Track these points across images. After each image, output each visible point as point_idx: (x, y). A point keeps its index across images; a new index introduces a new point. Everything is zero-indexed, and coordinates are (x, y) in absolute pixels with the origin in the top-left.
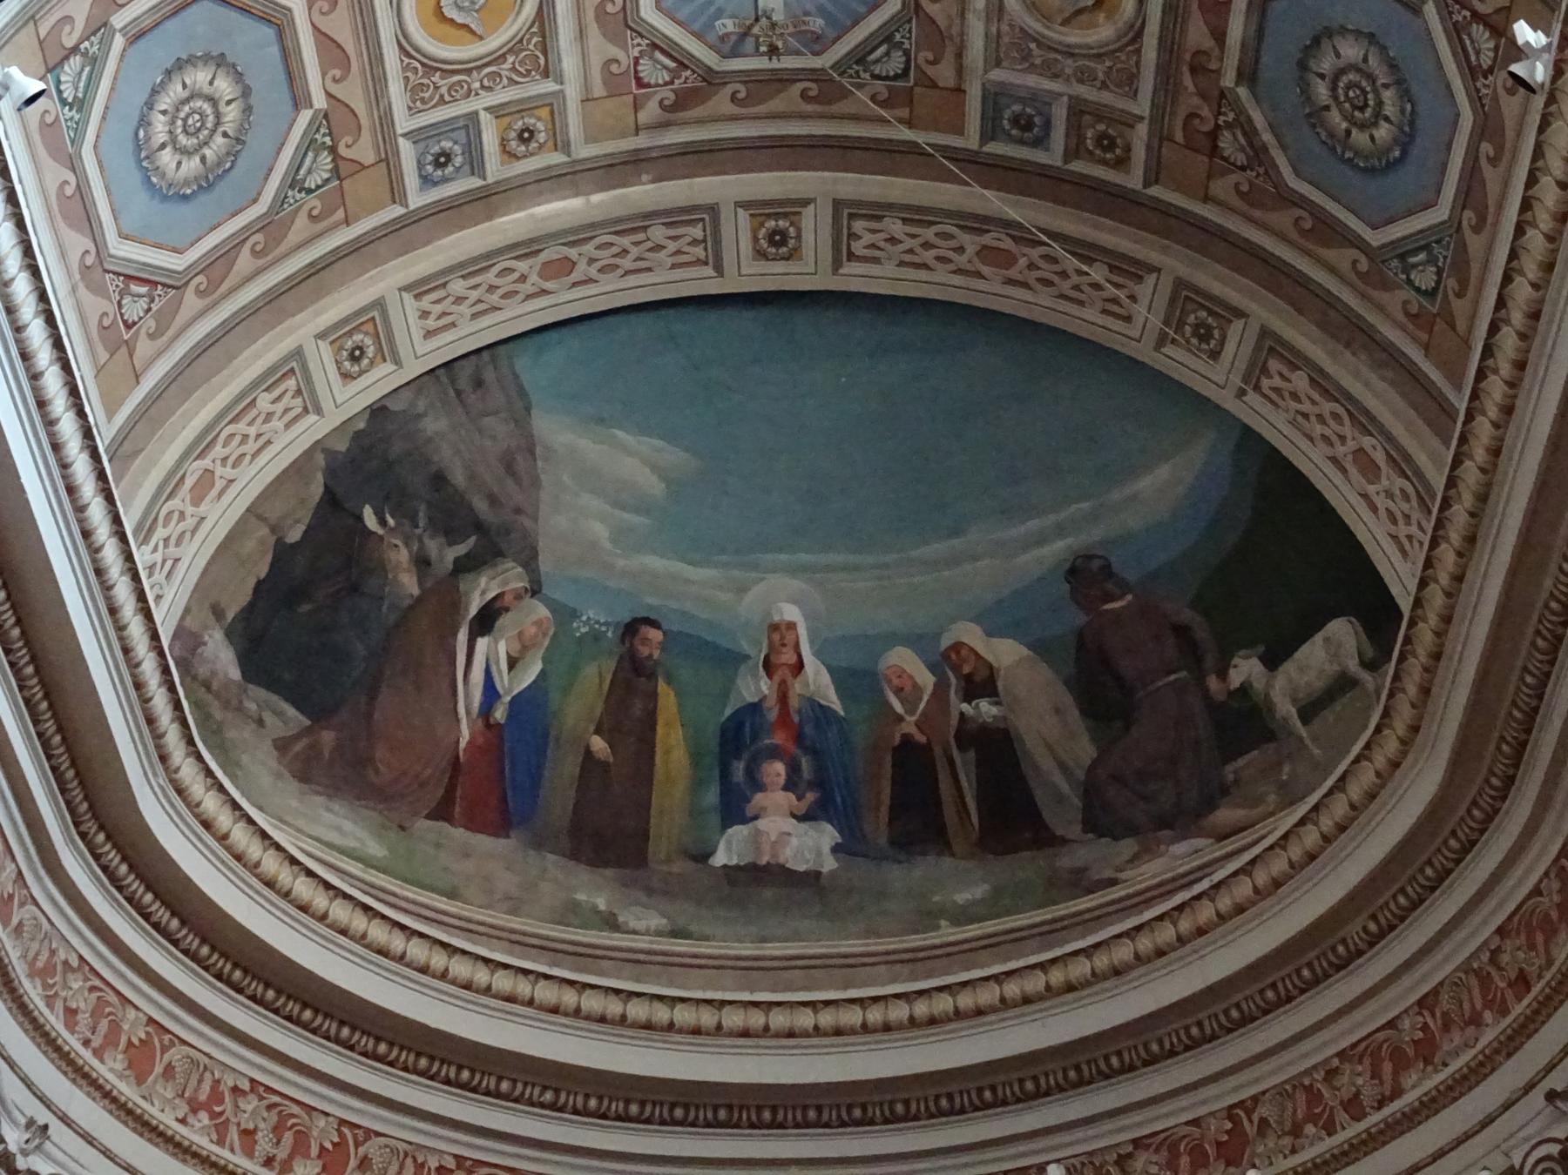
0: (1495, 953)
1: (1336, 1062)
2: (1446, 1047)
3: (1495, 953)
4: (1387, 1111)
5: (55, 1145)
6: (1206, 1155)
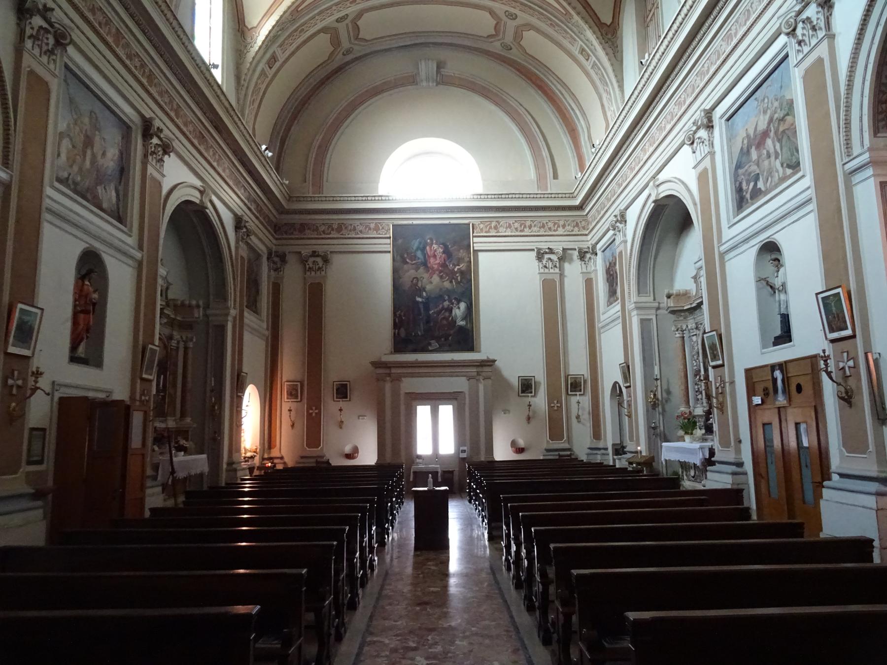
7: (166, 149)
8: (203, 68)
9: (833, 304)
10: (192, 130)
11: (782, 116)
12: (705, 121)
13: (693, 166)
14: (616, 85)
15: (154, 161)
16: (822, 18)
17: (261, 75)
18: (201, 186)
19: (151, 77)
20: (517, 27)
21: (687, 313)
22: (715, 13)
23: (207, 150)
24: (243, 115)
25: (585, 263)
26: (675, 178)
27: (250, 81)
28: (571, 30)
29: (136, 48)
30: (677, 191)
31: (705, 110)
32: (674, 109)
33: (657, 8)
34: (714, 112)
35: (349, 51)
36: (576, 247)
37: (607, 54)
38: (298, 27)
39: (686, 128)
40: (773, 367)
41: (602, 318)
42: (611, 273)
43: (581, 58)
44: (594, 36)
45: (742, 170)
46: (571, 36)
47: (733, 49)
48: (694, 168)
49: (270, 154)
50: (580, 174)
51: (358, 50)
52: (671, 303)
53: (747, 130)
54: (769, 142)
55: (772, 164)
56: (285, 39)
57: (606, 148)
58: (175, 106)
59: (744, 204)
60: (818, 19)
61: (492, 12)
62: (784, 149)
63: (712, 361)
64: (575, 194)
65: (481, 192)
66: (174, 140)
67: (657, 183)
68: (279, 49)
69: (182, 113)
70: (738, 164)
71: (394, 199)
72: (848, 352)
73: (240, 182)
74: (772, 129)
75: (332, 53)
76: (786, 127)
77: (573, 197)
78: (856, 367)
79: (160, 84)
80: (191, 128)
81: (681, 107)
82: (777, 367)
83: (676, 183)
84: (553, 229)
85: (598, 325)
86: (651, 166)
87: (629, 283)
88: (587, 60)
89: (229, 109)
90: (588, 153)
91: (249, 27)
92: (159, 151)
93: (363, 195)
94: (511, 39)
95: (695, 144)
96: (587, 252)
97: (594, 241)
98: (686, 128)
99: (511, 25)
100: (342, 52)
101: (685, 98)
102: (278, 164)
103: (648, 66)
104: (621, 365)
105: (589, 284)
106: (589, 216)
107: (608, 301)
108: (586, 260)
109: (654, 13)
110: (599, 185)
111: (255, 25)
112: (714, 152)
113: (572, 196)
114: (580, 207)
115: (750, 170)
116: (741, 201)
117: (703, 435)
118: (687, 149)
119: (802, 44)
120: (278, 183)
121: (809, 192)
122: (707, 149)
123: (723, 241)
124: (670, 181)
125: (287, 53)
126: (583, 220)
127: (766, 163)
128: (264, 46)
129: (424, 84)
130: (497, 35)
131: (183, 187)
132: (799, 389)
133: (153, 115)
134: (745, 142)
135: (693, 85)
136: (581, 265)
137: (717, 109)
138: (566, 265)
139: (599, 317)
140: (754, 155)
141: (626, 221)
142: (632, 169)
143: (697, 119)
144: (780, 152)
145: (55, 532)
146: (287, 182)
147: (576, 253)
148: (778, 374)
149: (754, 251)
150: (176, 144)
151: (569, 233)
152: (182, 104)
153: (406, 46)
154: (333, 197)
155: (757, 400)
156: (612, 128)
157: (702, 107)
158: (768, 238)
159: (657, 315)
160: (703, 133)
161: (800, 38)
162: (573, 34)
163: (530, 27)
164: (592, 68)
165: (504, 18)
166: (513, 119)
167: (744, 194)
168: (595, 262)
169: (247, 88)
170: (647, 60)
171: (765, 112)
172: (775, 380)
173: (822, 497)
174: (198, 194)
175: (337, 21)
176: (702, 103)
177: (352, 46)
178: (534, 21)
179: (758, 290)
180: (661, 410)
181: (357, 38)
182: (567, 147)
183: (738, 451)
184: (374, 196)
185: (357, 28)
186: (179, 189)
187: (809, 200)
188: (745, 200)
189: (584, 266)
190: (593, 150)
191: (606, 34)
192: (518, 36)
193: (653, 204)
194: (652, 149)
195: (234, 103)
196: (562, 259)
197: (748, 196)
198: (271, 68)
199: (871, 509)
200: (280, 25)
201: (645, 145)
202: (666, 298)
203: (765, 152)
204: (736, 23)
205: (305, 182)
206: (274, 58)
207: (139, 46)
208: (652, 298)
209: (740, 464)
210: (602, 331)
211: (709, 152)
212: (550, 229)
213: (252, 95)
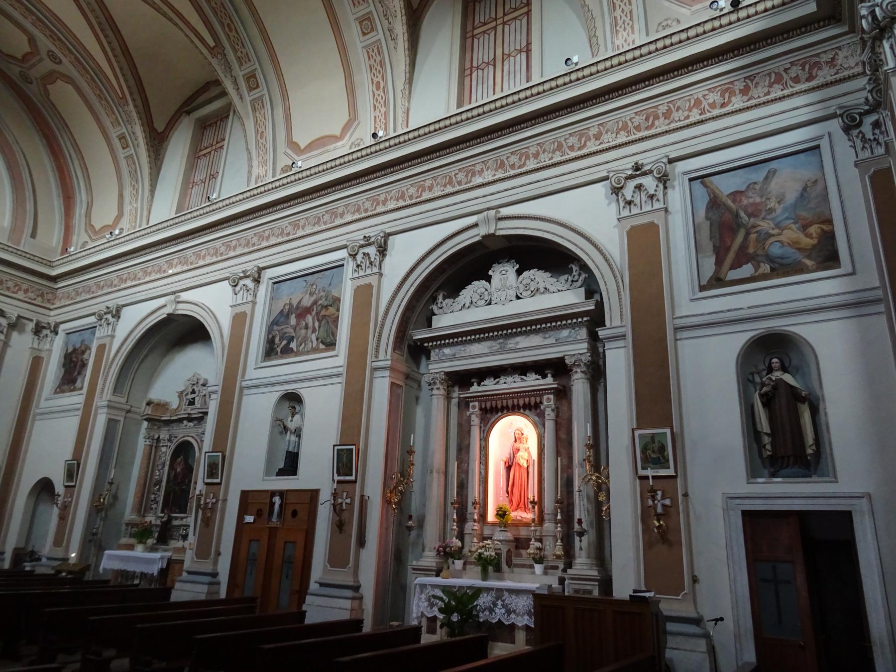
0: (323, 215)
1: (568, 136)
2: (436, 189)
3: (323, 215)
4: (466, 186)
5: (289, 446)
6: (590, 137)
9: (345, 455)
11: (325, 304)
12: (256, 276)
16: (378, 260)
21: (162, 424)
22: (292, 203)
25: (38, 339)
30: (202, 316)
36: (35, 319)
40: (273, 493)
41: (43, 404)
42: (74, 359)
43: (117, 143)
44: (144, 134)
45: (278, 327)
46: (117, 118)
52: (149, 411)
53: (291, 299)
54: (309, 318)
55: (308, 335)
59: (273, 354)
60: (375, 259)
61: (32, 40)
62: (322, 329)
63: (207, 478)
64: (54, 264)
70: (276, 321)
72: (347, 492)
74: (315, 309)
76: (327, 313)
77: (50, 266)
78: (351, 504)
82: (277, 494)
84: (12, 289)
85: (34, 410)
86: (177, 282)
87: (107, 376)
95: (238, 288)
96: (44, 328)
97: (59, 319)
104: (67, 462)
105: (36, 364)
106: (60, 291)
107: (59, 387)
108: (41, 335)
112: (256, 303)
113: (50, 264)
114: (54, 279)
115: (285, 330)
116: (270, 351)
117: (153, 544)
119: (360, 268)
121: (341, 369)
122: (250, 298)
123: (246, 378)
126: (51, 292)
127: (303, 331)
132: (294, 514)
134: (287, 307)
136: (33, 339)
138: (15, 335)
139: (39, 401)
140: (293, 320)
141: (119, 317)
144: (317, 329)
145: (621, 602)
147: (31, 326)
148: (277, 500)
149: (277, 396)
151: (30, 301)
155: (249, 519)
158: (294, 389)
159: (125, 418)
160: (249, 282)
161: (359, 263)
162: (119, 118)
167: (276, 346)
168: (52, 341)
171: (311, 294)
172: (272, 504)
173: (304, 602)
179: (273, 427)
180: (103, 515)
183: (215, 563)
187: (340, 375)
188: (275, 352)
189: (36, 342)
191: (154, 140)
192: (50, 77)
193: (166, 316)
196: (13, 326)
197: (279, 350)
199: (346, 609)
202: (144, 404)
203: (304, 323)
208: (126, 401)
209: (215, 575)
210: (37, 418)
212: (8, 289)
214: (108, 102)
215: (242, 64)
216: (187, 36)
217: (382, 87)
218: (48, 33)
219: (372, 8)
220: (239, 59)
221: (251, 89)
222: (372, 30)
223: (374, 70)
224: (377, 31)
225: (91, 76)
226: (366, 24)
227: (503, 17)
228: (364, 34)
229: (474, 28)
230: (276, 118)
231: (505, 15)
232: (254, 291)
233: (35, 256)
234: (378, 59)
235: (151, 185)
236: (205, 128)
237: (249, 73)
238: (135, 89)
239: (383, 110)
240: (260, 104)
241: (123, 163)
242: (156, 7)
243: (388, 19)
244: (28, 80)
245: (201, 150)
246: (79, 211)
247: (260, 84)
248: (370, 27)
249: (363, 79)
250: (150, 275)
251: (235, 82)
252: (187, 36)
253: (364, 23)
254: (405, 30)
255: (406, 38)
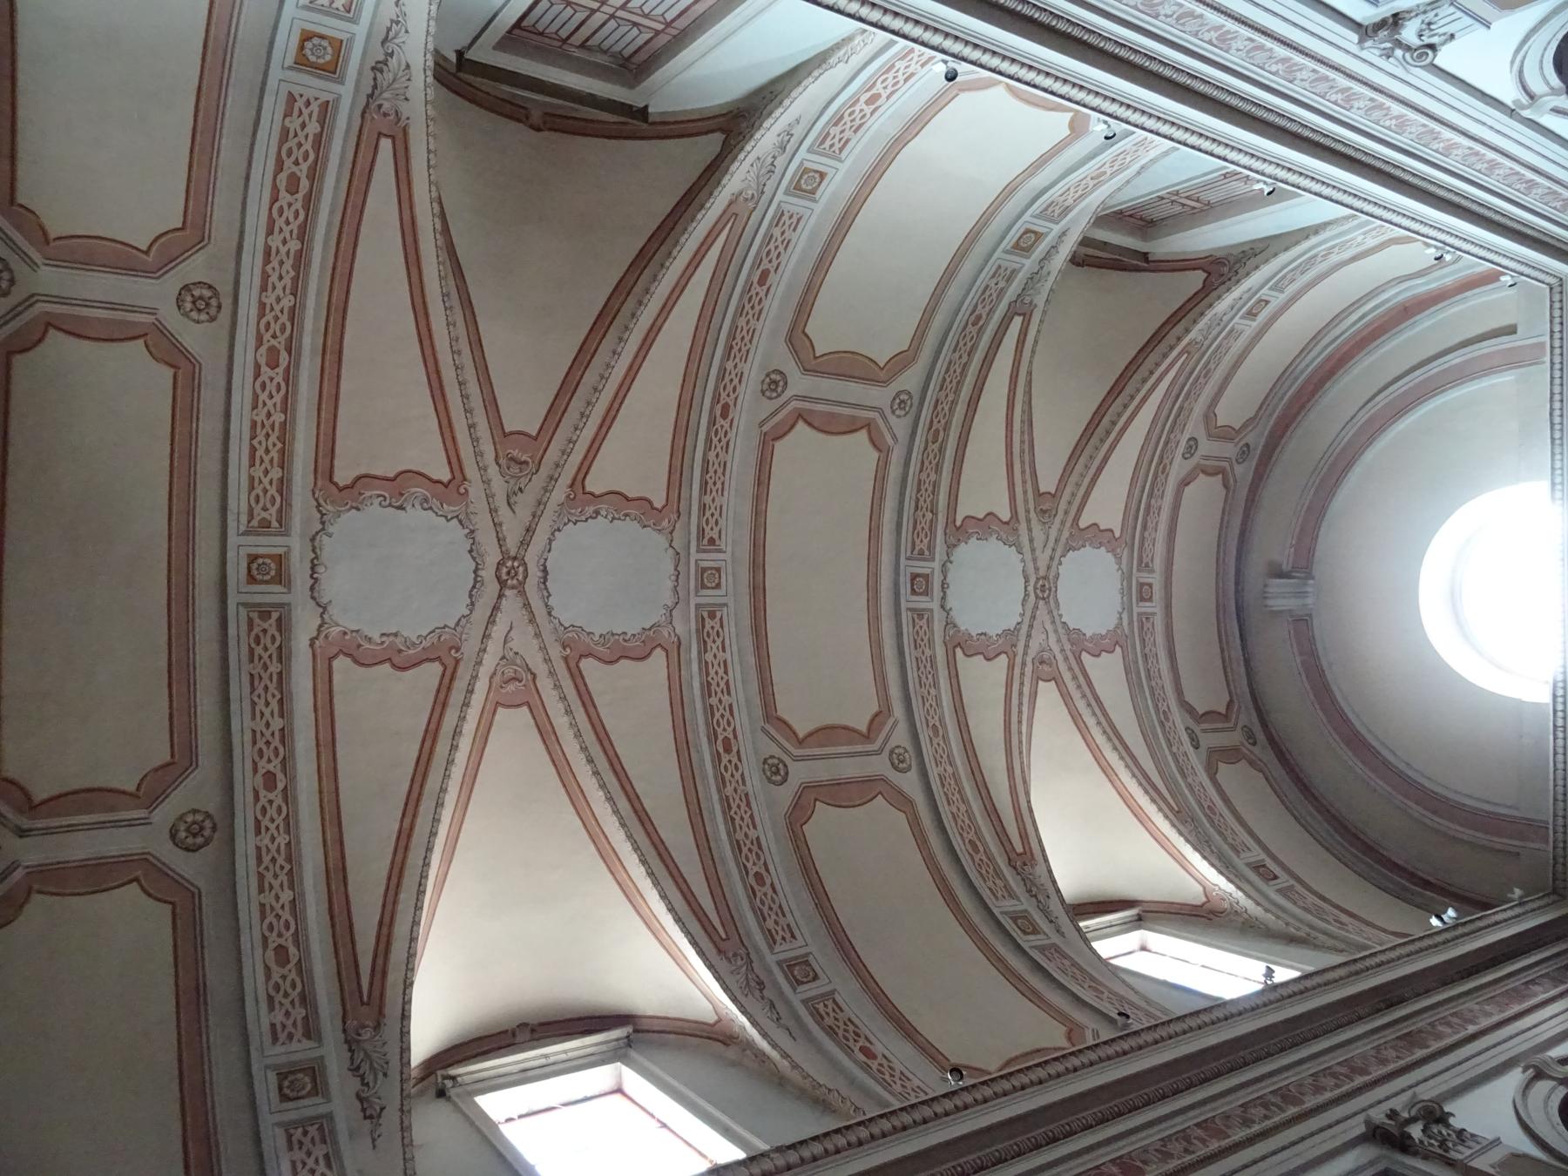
7: (1434, 1116)
8: (1273, 996)
10: (1264, 1111)
12: (1383, 34)
13: (1483, 29)
14: (1314, 240)
15: (1460, 1148)
17: (1285, 896)
18: (1524, 1072)
19: (1286, 1097)
20: (1210, 436)
23: (1439, 1037)
24: (1366, 947)
26: (1512, 62)
27: (1301, 921)
28: (1215, 339)
29: (1153, 1137)
30: (1545, 49)
31: (1361, 41)
32: (1238, 50)
33: (1177, 193)
34: (1366, 23)
35: (1251, 737)
37: (1257, 267)
38: (1206, 815)
39: (1399, 72)
46: (1225, 338)
47: (1411, 107)
48: (1487, 25)
49: (1451, 913)
50: (1503, 278)
51: (1248, 717)
56: (1225, 839)
57: (1444, 231)
58: (1343, 1070)
61: (1185, 482)
65: (1546, 484)
66: (1415, 1095)
67: (1525, 100)
68: (777, 948)
69: (1359, 1063)
71: (1561, 670)
73: (1514, 989)
75: (1252, 763)
79: (1301, 1085)
80: (1258, 1112)
81: (1296, 64)
83: (1524, 57)
88: (1267, 302)
89: (1354, 969)
90: (1473, 266)
91: (1204, 899)
92: (1440, 1133)
93: (1551, 737)
94: (1230, 445)
95: (1435, 40)
98: (1399, 72)
99: (1206, 447)
100: (1249, 747)
101: (1276, 63)
102: (1475, 902)
103: (1276, 179)
109: (1187, 198)
110: (1529, 232)
111: (1201, 889)
118: (1442, 59)
120: (1518, 910)
124: (1521, 72)
125: (1250, 842)
128: (1237, 880)
129: (1309, 601)
130: (868, 426)
131: (1526, 1106)
133: (1361, 1118)
135: (1248, 52)
137: (1358, 18)
142: (1493, 165)
143: (1377, 52)
146: (1518, 892)
150: (1427, 1092)
152: (1341, 1055)
153: (1241, 635)
154: (1555, 800)
156: (1409, 230)
157: (1354, 49)
160: (1409, 33)
163: (1209, 415)
164: (1282, 291)
165: (1195, 460)
166: (1382, 429)
169: (1312, 927)
170: (1265, 183)
174: (1543, 1086)
175: (1196, 747)
176: (1348, 52)
177: (1240, 725)
178: (1199, 408)
181: (1226, 717)
182: (1441, 317)
184: (1555, 711)
185: (1209, 715)
186: (1530, 1117)
190: (1448, 257)
194: (1447, 134)
195: (1340, 959)
198: (1276, 877)
200: (1203, 845)
201: (1436, 151)
204: (1200, 36)
205: (1518, 854)
206: (1258, 868)
207: (1228, 1099)
211: (1452, 4)
213: (1328, 922)
214: (1208, 362)
215: (1013, 271)
216: (1033, 352)
217: (868, 95)
218: (1161, 477)
219: (780, 196)
220: (1009, 280)
221: (1039, 236)
222: (806, 171)
223: (858, 122)
224: (801, 163)
225: (1183, 401)
226: (807, 184)
227: (598, 10)
228: (822, 175)
229: (657, 33)
230: (1055, 177)
231: (593, 11)
232: (1425, 12)
233: (1552, 317)
234: (835, 131)
235: (1307, 237)
236: (1152, 221)
237: (1017, 255)
238: (1162, 347)
239: (900, 65)
240: (1050, 209)
241: (1291, 289)
242: (1026, 408)
243: (772, 164)
244: (1246, 451)
245: (1194, 208)
246: (1422, 286)
247: (1022, 230)
248: (805, 177)
249: (883, 123)
250: (1492, 161)
251: (1047, 256)
252: (1033, 352)
253: (810, 188)
254: (762, 131)
255: (770, 121)
